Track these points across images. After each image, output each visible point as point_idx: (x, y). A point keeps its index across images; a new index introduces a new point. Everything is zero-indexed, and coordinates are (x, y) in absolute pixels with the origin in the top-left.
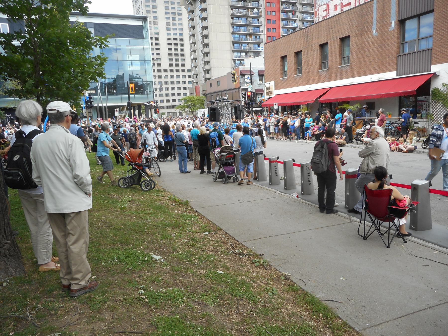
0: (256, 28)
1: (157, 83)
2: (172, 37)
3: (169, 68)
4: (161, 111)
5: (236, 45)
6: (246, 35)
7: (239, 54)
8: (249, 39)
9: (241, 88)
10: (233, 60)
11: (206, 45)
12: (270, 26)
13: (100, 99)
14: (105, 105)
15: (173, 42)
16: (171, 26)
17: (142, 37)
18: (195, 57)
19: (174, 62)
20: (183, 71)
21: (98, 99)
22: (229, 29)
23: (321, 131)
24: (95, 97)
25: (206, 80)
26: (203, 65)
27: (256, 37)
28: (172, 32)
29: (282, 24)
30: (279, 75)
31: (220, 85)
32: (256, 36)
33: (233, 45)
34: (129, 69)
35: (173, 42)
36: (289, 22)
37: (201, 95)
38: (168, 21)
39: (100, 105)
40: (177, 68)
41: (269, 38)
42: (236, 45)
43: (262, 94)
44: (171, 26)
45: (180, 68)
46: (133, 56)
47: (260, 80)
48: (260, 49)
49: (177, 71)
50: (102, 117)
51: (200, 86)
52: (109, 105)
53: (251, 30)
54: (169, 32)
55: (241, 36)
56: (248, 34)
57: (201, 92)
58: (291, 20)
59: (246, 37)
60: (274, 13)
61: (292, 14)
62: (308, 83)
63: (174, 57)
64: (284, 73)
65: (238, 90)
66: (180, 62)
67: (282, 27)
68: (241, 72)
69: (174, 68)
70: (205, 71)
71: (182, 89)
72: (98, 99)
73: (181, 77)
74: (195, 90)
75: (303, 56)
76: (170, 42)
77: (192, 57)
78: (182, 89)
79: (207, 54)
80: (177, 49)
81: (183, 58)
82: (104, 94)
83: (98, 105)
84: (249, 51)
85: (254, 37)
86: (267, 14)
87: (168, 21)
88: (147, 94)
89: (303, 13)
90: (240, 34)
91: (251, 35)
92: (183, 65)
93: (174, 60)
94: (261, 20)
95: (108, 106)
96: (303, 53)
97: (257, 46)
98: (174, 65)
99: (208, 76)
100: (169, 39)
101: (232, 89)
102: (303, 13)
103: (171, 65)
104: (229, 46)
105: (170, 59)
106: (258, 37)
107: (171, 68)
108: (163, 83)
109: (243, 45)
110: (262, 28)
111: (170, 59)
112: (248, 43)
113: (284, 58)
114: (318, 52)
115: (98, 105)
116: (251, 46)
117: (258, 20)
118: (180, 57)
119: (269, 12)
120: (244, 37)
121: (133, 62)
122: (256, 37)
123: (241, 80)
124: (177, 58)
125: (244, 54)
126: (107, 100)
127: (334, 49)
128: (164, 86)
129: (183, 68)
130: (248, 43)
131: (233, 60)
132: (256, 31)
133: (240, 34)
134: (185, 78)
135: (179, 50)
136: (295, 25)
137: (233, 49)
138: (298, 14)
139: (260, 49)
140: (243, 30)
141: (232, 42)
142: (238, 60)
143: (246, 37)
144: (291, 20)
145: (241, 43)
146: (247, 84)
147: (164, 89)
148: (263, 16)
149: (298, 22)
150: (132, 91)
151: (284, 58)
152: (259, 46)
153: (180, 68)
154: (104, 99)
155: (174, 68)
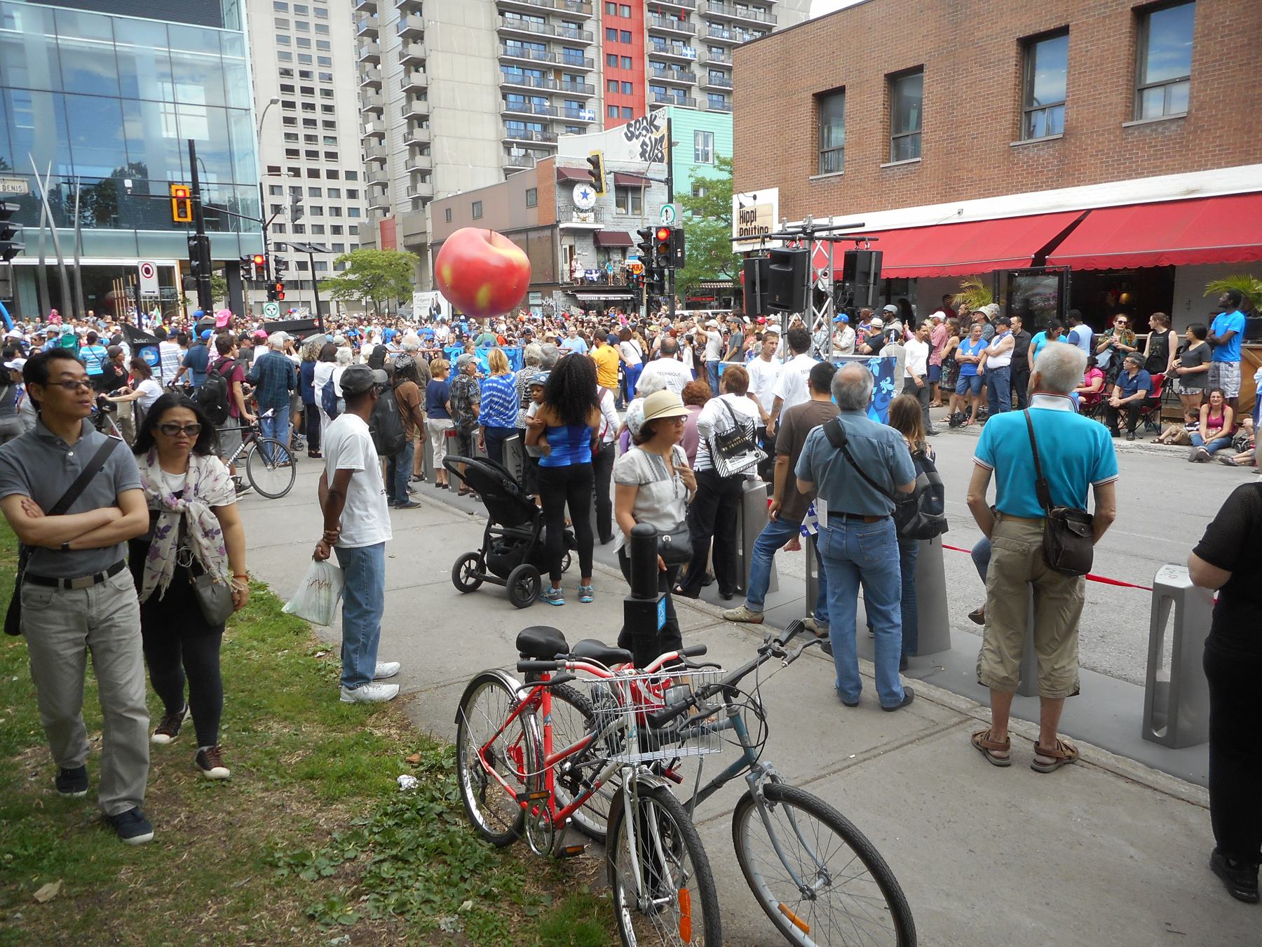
0: (572, 52)
1: (286, 191)
2: (296, 66)
3: (285, 163)
4: (290, 295)
5: (511, 98)
6: (544, 70)
7: (522, 126)
8: (552, 84)
9: (561, 226)
10: (504, 143)
11: (419, 93)
12: (618, 48)
13: (50, 239)
14: (69, 261)
15: (297, 82)
16: (293, 33)
17: (219, 24)
18: (380, 129)
19: (302, 146)
20: (332, 175)
21: (42, 239)
22: (490, 47)
23: (1141, 393)
24: (30, 230)
25: (416, 202)
26: (406, 156)
27: (573, 79)
28: (294, 49)
29: (650, 46)
30: (805, 164)
31: (480, 216)
32: (576, 75)
33: (504, 97)
34: (165, 135)
35: (297, 82)
36: (668, 42)
37: (401, 250)
38: (282, 15)
39: (51, 261)
40: (313, 165)
41: (612, 84)
42: (511, 98)
43: (624, 251)
44: (293, 33)
45: (323, 165)
46: (179, 87)
47: (618, 205)
48: (585, 115)
49: (314, 173)
50: (57, 303)
51: (398, 220)
52: (85, 261)
53: (559, 57)
54: (284, 49)
55: (528, 73)
56: (550, 68)
57: (400, 239)
58: (676, 37)
59: (544, 74)
60: (627, 9)
61: (680, 19)
62: (949, 194)
63: (301, 130)
64: (823, 154)
65: (548, 233)
66: (321, 147)
67: (651, 56)
68: (560, 172)
69: (303, 164)
70: (414, 173)
71: (328, 230)
72: (42, 239)
73: (325, 192)
74: (378, 233)
75: (930, 92)
76: (287, 82)
77: (370, 128)
78: (328, 230)
79: (421, 120)
80: (311, 107)
81: (330, 133)
82: (64, 221)
83: (42, 261)
84: (552, 121)
85: (566, 78)
86: (606, 12)
87: (282, 15)
88: (238, 230)
89: (712, 19)
90: (524, 66)
91: (558, 71)
92: (332, 156)
93: (301, 138)
94: (589, 26)
95: (85, 269)
96: (927, 76)
97: (575, 105)
98: (302, 154)
99: (423, 190)
100: (286, 73)
101: (527, 231)
102: (712, 19)
103: (292, 153)
104: (490, 101)
105: (288, 136)
106: (579, 80)
107: (294, 163)
108: (305, 192)
109: (535, 100)
110: (590, 53)
111: (288, 136)
112: (549, 96)
113: (826, 100)
114: (1012, 69)
115: (42, 261)
116: (560, 104)
117: (580, 27)
118: (320, 132)
119: (612, 6)
120: (536, 74)
121: (181, 108)
122: (573, 79)
123: (560, 200)
124: (311, 132)
125: (538, 127)
126: (80, 246)
127: (866, 108)
128: (307, 202)
129: (332, 166)
130: (549, 96)
131: (504, 143)
132: (572, 59)
133: (524, 66)
134: (339, 197)
135: (318, 108)
136: (688, 53)
137: (503, 110)
138: (694, 19)
139: (585, 115)
140: (534, 54)
141: (502, 88)
142: (520, 145)
143: (544, 74)
144: (676, 37)
145: (528, 94)
146: (582, 215)
147: (307, 210)
148: (594, 17)
149: (694, 43)
150: (182, 211)
151: (826, 100)
152: (582, 107)
153: (323, 165)
154: (64, 239)
155: (303, 164)
